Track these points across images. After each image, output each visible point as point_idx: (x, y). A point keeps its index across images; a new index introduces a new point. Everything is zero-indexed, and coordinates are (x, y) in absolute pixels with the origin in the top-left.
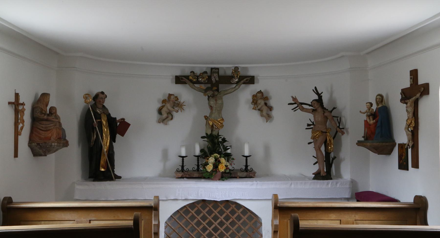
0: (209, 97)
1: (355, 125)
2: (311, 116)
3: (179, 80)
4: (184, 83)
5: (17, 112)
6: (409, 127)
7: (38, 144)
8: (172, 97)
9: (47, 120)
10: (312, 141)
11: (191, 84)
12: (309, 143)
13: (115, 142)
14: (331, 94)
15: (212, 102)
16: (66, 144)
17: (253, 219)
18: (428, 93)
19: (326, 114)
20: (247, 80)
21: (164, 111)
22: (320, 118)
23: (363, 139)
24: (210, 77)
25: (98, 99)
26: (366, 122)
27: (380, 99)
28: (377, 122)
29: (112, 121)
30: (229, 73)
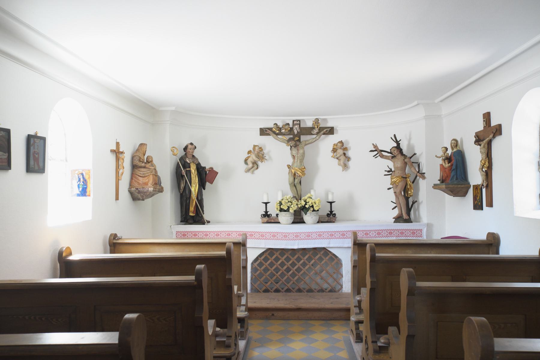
0: (291, 147)
1: (432, 168)
2: (390, 164)
3: (263, 132)
4: (269, 135)
5: (117, 159)
6: (483, 168)
7: (137, 189)
8: (257, 148)
9: (145, 167)
10: (391, 186)
11: (275, 135)
12: (389, 189)
13: (204, 189)
15: (294, 152)
16: (161, 190)
17: (336, 261)
18: (501, 134)
19: (406, 160)
20: (327, 131)
21: (249, 162)
22: (399, 164)
23: (439, 182)
24: (292, 129)
26: (441, 165)
27: (455, 143)
28: (452, 165)
29: (201, 170)
30: (309, 124)
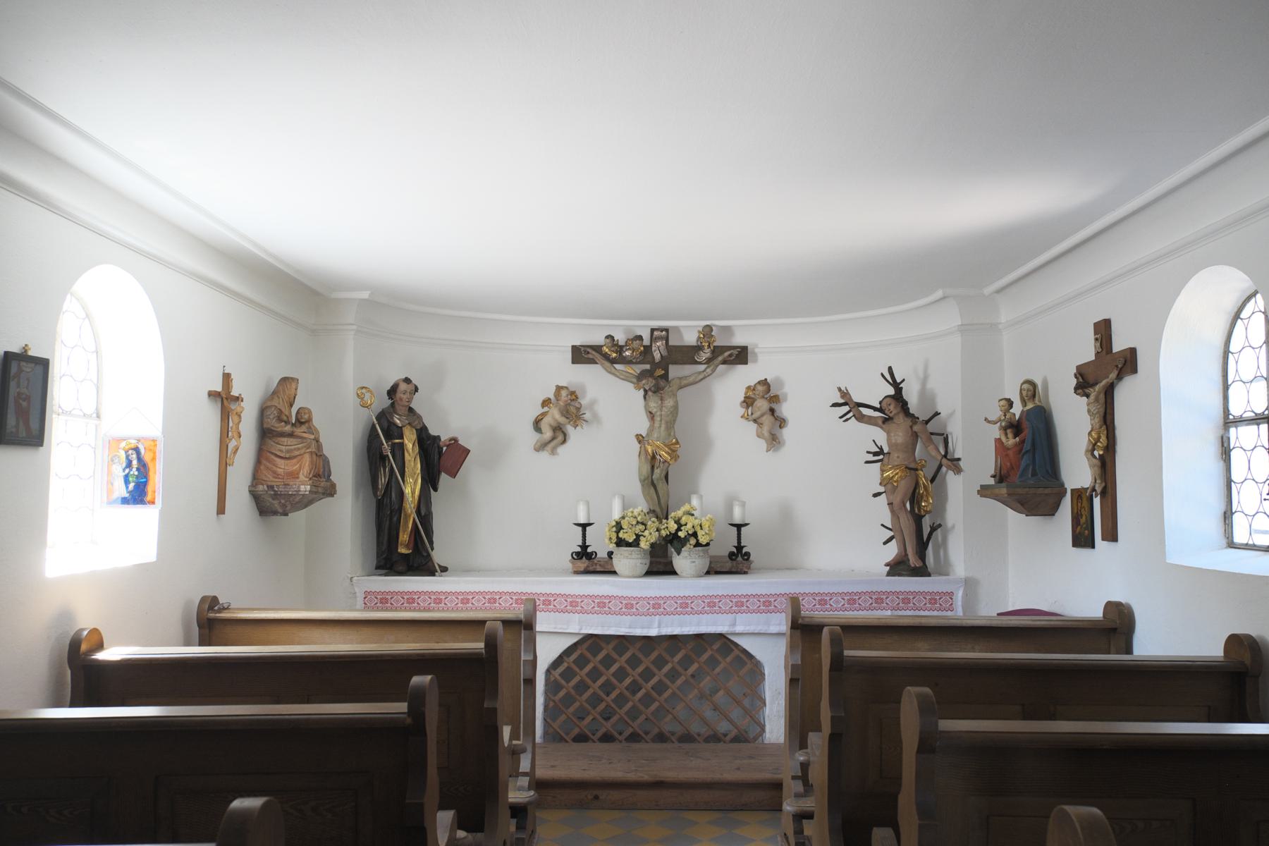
0: (646, 391)
1: (977, 448)
2: (879, 436)
3: (581, 355)
5: (225, 415)
7: (270, 487)
8: (564, 393)
9: (291, 435)
10: (882, 489)
11: (607, 364)
12: (876, 495)
13: (436, 490)
14: (924, 381)
16: (330, 491)
17: (749, 666)
18: (1134, 370)
19: (916, 428)
20: (730, 355)
21: (545, 425)
22: (900, 436)
23: (992, 482)
24: (648, 349)
25: (399, 396)
26: (998, 441)
27: (1031, 390)
28: (1023, 442)
